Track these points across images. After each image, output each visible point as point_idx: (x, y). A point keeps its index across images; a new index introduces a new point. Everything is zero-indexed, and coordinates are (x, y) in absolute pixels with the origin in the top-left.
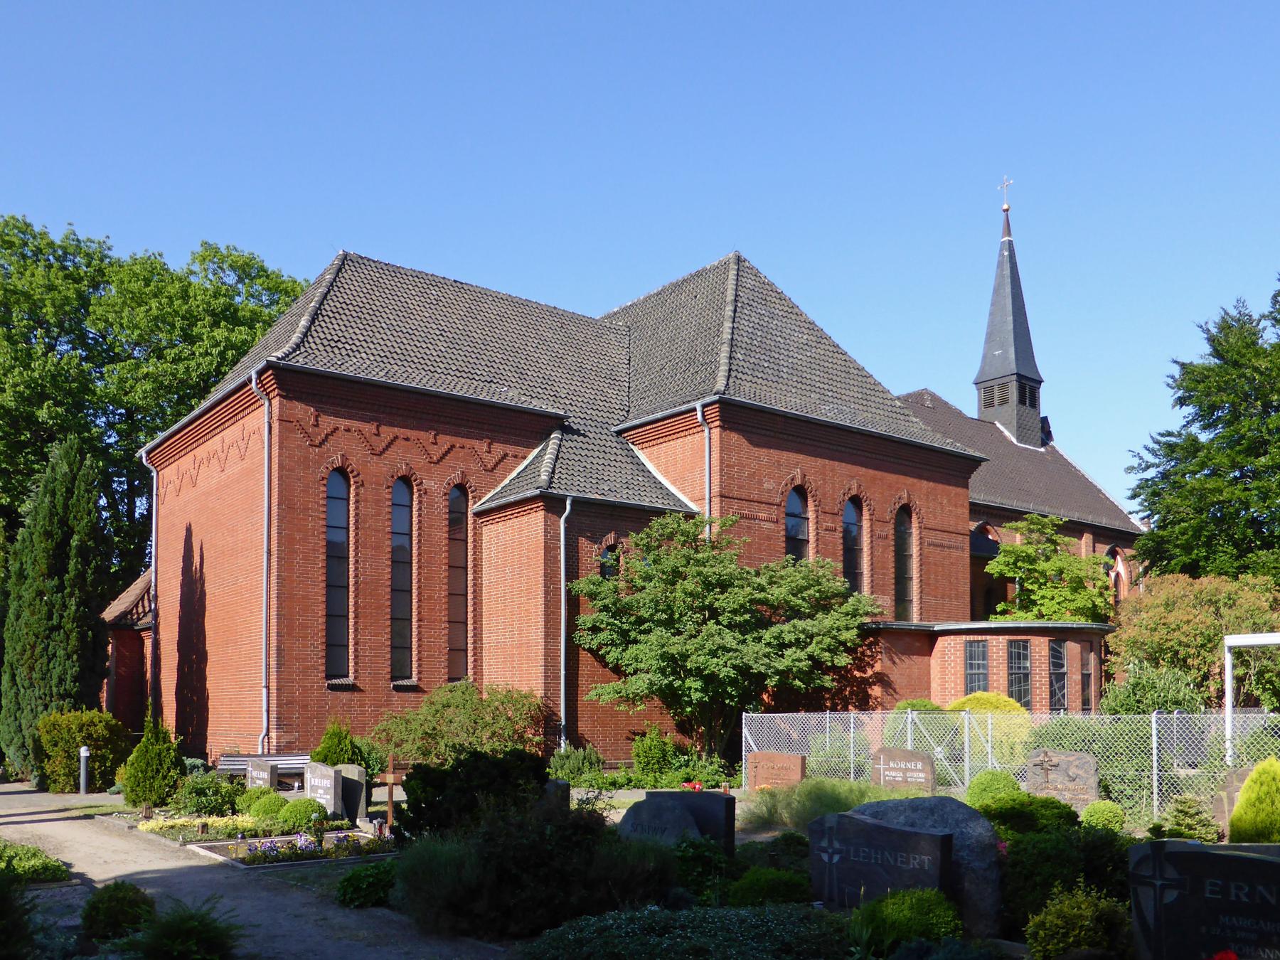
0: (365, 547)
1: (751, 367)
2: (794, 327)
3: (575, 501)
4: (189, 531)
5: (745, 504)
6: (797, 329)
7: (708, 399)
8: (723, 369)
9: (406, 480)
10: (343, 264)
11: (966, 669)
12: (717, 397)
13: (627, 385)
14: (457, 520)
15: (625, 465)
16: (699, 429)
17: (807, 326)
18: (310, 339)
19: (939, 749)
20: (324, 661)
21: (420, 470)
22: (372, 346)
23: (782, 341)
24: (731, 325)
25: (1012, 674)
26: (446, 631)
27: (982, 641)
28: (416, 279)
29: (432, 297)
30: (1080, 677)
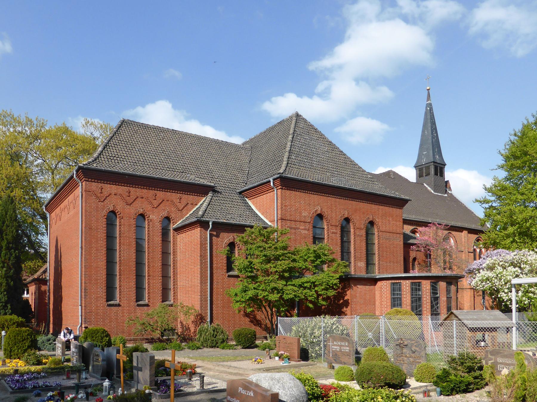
0: (124, 245)
1: (298, 162)
2: (322, 144)
3: (214, 223)
4: (57, 238)
5: (294, 223)
6: (323, 145)
7: (275, 177)
8: (285, 163)
9: (142, 216)
10: (122, 124)
11: (391, 295)
12: (279, 175)
13: (247, 172)
14: (165, 233)
15: (242, 207)
16: (273, 190)
17: (327, 143)
18: (102, 156)
19: (370, 333)
20: (105, 294)
21: (148, 211)
22: (130, 158)
23: (315, 150)
24: (290, 144)
25: (413, 298)
26: (161, 281)
27: (399, 283)
28: (155, 130)
29: (161, 137)
30: (446, 299)
